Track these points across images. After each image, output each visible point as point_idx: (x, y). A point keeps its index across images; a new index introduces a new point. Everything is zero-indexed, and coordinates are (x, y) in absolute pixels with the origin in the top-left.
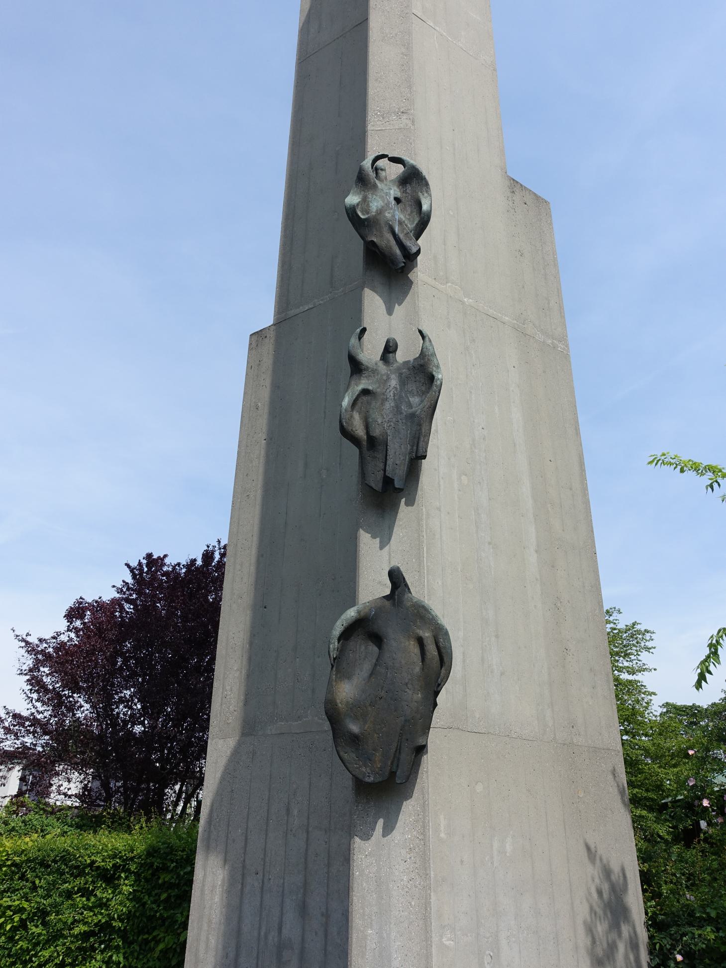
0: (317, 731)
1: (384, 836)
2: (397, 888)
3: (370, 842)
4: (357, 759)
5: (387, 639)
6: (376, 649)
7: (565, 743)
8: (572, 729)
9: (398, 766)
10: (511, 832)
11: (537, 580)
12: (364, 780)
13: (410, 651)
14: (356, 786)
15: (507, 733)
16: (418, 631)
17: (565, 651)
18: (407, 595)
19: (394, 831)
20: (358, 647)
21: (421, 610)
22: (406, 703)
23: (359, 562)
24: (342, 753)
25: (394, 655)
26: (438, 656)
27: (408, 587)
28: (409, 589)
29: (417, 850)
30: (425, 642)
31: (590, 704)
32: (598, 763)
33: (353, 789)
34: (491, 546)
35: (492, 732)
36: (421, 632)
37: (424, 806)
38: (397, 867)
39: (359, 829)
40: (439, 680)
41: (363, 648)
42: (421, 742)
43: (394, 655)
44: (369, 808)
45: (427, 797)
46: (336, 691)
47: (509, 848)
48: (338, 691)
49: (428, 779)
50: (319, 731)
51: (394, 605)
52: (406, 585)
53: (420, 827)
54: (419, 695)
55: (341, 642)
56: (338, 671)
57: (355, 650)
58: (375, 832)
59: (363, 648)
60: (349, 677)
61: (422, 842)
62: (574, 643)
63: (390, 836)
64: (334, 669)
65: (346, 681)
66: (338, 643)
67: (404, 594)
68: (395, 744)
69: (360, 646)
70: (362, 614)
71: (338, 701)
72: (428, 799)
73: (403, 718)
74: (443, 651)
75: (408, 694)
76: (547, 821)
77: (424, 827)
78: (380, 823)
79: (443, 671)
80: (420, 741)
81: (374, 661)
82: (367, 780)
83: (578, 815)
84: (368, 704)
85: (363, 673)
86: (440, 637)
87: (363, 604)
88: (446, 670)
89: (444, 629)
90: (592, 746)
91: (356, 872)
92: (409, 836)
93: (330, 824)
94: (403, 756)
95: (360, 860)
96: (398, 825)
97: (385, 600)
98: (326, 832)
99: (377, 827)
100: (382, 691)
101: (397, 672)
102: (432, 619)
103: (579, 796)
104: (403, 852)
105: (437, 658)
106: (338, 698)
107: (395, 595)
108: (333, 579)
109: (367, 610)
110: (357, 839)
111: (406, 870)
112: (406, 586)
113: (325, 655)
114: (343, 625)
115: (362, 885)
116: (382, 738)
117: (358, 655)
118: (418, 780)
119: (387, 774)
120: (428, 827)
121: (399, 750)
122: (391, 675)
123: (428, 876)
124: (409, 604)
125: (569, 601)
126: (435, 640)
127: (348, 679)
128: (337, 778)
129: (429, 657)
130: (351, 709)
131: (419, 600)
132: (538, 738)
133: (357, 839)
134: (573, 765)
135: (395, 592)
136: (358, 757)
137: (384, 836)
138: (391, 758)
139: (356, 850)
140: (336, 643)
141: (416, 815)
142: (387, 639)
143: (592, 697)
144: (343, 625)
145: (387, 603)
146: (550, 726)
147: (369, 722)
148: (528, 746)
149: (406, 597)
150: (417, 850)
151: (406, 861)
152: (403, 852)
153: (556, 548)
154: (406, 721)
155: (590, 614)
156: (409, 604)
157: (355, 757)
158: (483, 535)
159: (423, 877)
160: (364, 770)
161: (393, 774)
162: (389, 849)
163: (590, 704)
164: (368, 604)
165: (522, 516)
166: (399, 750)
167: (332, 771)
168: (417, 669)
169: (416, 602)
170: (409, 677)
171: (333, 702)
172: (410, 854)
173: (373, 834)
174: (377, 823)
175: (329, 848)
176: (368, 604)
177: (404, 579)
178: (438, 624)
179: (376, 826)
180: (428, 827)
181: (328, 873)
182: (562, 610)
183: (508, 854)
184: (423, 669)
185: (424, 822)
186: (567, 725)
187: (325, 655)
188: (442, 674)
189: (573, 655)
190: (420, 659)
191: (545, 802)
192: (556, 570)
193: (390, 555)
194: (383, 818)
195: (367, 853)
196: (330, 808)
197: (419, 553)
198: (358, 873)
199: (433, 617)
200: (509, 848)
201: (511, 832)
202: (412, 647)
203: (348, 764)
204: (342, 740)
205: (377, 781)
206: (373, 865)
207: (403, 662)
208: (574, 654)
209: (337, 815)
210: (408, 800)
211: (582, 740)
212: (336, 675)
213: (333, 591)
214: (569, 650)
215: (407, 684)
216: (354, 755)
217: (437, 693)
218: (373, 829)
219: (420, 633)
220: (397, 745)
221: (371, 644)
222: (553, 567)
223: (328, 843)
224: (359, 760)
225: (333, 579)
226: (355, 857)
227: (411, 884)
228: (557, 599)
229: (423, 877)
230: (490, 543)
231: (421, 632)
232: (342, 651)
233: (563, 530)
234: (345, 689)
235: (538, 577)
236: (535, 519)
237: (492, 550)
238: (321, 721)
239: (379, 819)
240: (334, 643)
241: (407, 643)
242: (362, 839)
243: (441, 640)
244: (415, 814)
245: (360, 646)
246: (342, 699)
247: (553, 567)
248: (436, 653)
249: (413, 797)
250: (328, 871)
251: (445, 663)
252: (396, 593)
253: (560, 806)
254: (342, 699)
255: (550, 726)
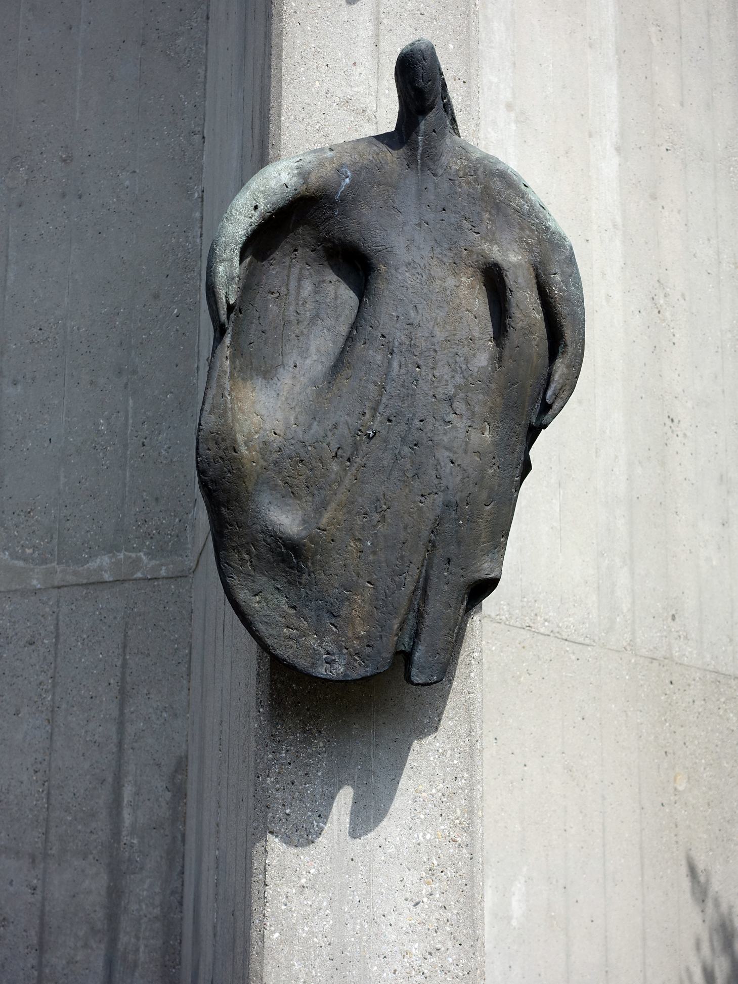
0: (9, 592)
1: (355, 833)
2: (391, 975)
3: (312, 850)
4: (293, 611)
5: (386, 264)
6: (348, 295)
7: (655, 656)
8: (672, 624)
9: (417, 634)
10: (525, 869)
11: (615, 226)
12: (313, 671)
13: (459, 305)
14: (271, 695)
15: (528, 621)
16: (486, 246)
17: (668, 422)
18: (449, 140)
19: (385, 822)
20: (293, 284)
21: (498, 184)
22: (447, 454)
23: (280, 35)
24: (243, 595)
25: (412, 314)
26: (543, 326)
27: (453, 113)
28: (454, 121)
29: (450, 872)
30: (510, 281)
31: (714, 563)
32: (721, 712)
33: (260, 704)
34: (513, 115)
35: (493, 615)
36: (495, 248)
37: (471, 753)
38: (392, 918)
39: (280, 814)
40: (550, 393)
41: (308, 288)
42: (485, 570)
43: (412, 314)
44: (310, 756)
45: (479, 732)
46: (232, 409)
47: (517, 908)
48: (240, 409)
49: (481, 683)
50: (16, 591)
51: (411, 162)
52: (448, 108)
53: (458, 811)
54: (487, 434)
55: (248, 260)
56: (237, 351)
57: (283, 291)
58: (328, 824)
59: (308, 288)
60: (268, 373)
61: (464, 851)
62: (689, 405)
63: (373, 834)
64: (227, 340)
65: (260, 382)
66: (241, 262)
67: (444, 135)
68: (414, 571)
69: (300, 280)
70: (313, 180)
71: (240, 438)
72: (481, 737)
73: (439, 499)
74: (563, 309)
75: (455, 427)
76: (604, 846)
77: (470, 811)
78: (345, 798)
79: (560, 368)
80: (485, 565)
81: (344, 329)
82: (322, 671)
83: (673, 835)
84: (328, 455)
85: (308, 362)
86: (555, 268)
87: (315, 151)
88: (568, 367)
89: (564, 247)
90: (711, 668)
91: (273, 933)
92: (428, 836)
93: (46, 840)
94: (435, 608)
95: (284, 900)
96: (397, 803)
97: (381, 145)
98: (33, 861)
99: (334, 810)
100: (374, 416)
101: (420, 362)
102: (529, 214)
103: (676, 789)
104: (412, 877)
105: (541, 330)
106: (238, 428)
107: (417, 133)
108: (64, 161)
109: (328, 171)
110: (275, 843)
111: (419, 928)
112: (446, 111)
113: (33, 379)
114: (256, 208)
115: (289, 967)
116: (374, 553)
117: (292, 308)
118: (455, 683)
119: (387, 655)
120: (480, 813)
121: (423, 590)
122: (403, 371)
123: (479, 942)
124: (456, 165)
125: (683, 295)
126: (537, 277)
127: (265, 378)
128: (70, 718)
129: (520, 325)
130: (276, 463)
131: (487, 157)
132: (596, 638)
133: (275, 843)
134: (668, 713)
135: (417, 124)
136: (294, 607)
137: (355, 833)
138: (403, 611)
139: (271, 872)
140: (237, 260)
141: (449, 778)
142: (386, 264)
143: (719, 548)
144: (256, 208)
145: (392, 158)
146: (625, 610)
147: (333, 504)
148: (573, 657)
149: (448, 140)
150: (450, 872)
151: (417, 904)
152: (412, 877)
153: (663, 148)
154: (447, 505)
155: (729, 335)
156: (456, 165)
157: (286, 608)
158: (496, 80)
159: (466, 946)
160: (313, 642)
161: (404, 658)
162: (371, 870)
163: (714, 563)
164: (330, 154)
165: (591, 46)
166: (423, 590)
167: (53, 700)
168: (482, 359)
169: (478, 160)
170: (459, 379)
171: (224, 440)
172: (429, 883)
173: (322, 829)
174: (333, 798)
175: (43, 905)
176: (330, 154)
177: (444, 86)
178: (548, 228)
179: (331, 808)
180: (480, 813)
181: (40, 967)
182: (668, 315)
183: (514, 923)
184: (500, 359)
185: (470, 799)
186: (661, 611)
187: (33, 379)
188: (556, 377)
189: (685, 435)
190: (490, 330)
191: (604, 798)
192: (660, 209)
193: (378, 22)
194: (353, 787)
195: (303, 881)
196: (48, 799)
197: (468, 26)
198: (277, 935)
199: (532, 207)
200: (517, 908)
201: (525, 869)
202: (463, 292)
203: (261, 627)
204: (246, 557)
205: (354, 675)
206: (322, 913)
207: (440, 336)
208: (689, 434)
209: (69, 818)
210: (426, 735)
211: (691, 653)
212: (233, 357)
213: (64, 195)
214: (676, 421)
215: (450, 400)
216: (282, 602)
217: (533, 433)
218: (323, 816)
219: (495, 253)
220: (421, 572)
221: (334, 277)
222: (654, 197)
223: (38, 891)
224: (299, 615)
225: (64, 161)
226: (269, 892)
227: (433, 965)
228: (657, 285)
229: (466, 946)
230: (509, 107)
231: (495, 248)
232: (248, 286)
233: (682, 104)
234: (258, 407)
235: (619, 220)
236: (619, 60)
237: (514, 128)
238: (21, 564)
239: (340, 788)
240: (231, 260)
241: (451, 282)
242: (288, 840)
243: (558, 278)
244: (446, 774)
245: (300, 280)
246: (250, 433)
247: (654, 197)
248: (539, 317)
249: (441, 728)
250: (40, 963)
251: (566, 345)
252: (422, 126)
253: (634, 811)
254: (250, 433)
255: (625, 610)
